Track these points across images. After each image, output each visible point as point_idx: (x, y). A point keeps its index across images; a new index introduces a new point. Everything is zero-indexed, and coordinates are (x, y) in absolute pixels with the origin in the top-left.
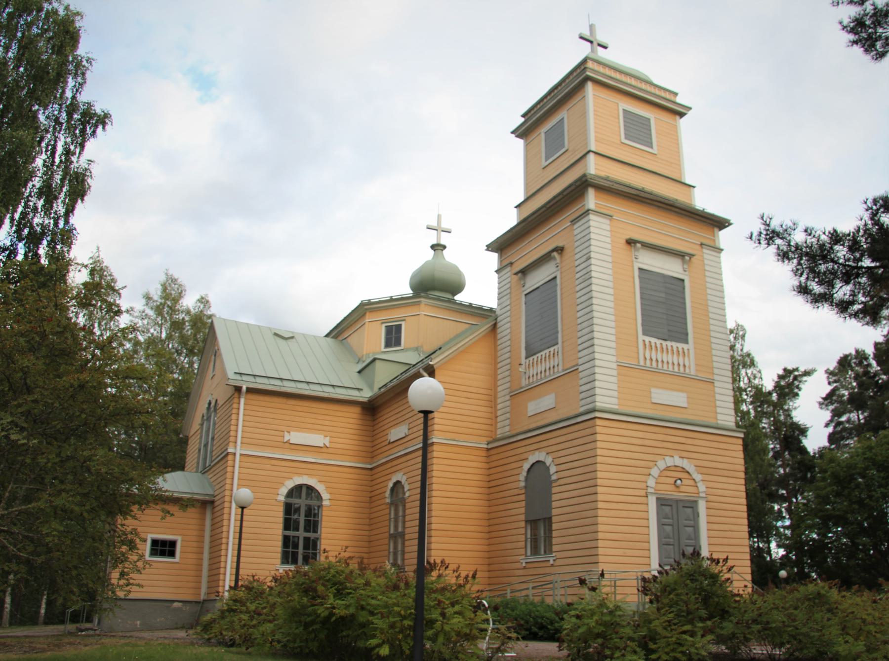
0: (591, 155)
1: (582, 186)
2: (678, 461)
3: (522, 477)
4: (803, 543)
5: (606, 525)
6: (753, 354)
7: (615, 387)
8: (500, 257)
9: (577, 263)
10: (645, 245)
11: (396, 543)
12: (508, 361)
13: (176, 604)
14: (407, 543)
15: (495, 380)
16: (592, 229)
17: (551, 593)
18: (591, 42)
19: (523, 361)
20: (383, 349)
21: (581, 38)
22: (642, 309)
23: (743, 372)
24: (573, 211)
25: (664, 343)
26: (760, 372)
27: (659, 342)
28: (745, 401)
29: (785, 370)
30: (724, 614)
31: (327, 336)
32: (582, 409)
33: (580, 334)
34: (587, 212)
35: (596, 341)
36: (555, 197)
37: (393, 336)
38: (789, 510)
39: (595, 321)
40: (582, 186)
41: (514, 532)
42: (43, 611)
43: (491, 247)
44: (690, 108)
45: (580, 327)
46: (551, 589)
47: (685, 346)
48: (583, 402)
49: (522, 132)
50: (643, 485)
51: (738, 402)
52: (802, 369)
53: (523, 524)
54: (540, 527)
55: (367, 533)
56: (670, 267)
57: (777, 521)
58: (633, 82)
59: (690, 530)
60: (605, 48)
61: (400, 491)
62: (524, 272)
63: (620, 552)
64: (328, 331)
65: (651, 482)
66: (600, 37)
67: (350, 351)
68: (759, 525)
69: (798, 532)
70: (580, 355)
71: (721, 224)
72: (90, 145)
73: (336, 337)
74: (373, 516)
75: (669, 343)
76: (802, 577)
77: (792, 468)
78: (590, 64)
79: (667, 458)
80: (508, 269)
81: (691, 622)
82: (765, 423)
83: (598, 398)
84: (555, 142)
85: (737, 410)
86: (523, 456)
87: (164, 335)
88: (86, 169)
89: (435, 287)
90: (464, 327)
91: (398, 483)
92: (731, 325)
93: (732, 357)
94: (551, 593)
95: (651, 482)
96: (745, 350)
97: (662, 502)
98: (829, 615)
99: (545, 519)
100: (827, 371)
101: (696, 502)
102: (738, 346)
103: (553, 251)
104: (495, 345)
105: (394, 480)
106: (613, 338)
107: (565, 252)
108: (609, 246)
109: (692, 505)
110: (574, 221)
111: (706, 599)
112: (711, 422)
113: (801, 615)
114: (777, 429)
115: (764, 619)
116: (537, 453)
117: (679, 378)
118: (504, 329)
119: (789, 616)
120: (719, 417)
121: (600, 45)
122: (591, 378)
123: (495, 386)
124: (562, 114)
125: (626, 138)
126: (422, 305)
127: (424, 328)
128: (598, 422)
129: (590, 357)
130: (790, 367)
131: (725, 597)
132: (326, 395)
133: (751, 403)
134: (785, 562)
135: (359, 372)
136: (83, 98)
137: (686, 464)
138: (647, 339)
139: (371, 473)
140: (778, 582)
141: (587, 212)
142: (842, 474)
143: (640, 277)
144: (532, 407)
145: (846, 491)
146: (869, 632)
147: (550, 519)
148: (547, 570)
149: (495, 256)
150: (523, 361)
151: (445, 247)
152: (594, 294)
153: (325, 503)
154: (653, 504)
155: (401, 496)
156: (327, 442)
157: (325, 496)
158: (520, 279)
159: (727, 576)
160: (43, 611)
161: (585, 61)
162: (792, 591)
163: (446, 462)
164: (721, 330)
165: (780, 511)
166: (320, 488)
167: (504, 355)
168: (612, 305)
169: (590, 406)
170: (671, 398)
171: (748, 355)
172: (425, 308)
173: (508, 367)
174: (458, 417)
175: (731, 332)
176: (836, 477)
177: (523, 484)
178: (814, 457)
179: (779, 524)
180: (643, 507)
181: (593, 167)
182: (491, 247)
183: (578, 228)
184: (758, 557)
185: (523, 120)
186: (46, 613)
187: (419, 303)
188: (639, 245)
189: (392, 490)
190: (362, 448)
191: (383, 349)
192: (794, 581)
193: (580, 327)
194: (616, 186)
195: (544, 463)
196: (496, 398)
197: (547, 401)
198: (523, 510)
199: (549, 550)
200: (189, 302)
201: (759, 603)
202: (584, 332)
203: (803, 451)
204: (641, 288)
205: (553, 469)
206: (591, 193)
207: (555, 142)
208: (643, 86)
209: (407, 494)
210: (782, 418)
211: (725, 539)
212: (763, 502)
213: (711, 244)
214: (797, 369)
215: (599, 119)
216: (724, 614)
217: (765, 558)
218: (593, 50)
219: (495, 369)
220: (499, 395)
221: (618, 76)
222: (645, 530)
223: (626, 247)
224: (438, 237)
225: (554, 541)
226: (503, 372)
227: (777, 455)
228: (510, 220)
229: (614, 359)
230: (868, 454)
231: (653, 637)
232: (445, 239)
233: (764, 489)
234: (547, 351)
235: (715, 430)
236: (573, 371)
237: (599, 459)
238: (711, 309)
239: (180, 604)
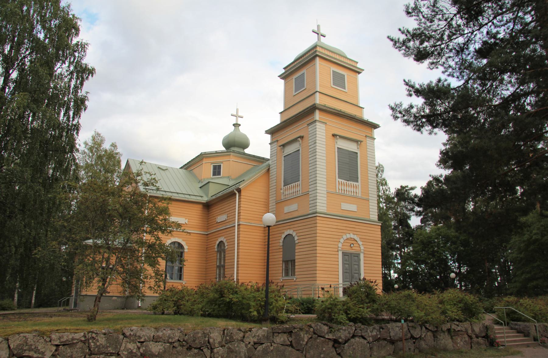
0: (318, 93)
1: (313, 109)
2: (352, 236)
3: (281, 241)
4: (406, 272)
5: (320, 264)
6: (386, 179)
7: (325, 202)
8: (272, 137)
9: (310, 144)
10: (341, 137)
11: (220, 270)
12: (275, 187)
13: (114, 298)
14: (226, 270)
15: (268, 196)
16: (317, 129)
17: (296, 293)
18: (318, 34)
19: (282, 187)
20: (212, 177)
21: (313, 32)
22: (338, 167)
23: (381, 188)
24: (308, 120)
25: (348, 182)
26: (389, 188)
27: (345, 182)
28: (381, 202)
29: (401, 187)
30: (374, 301)
31: (181, 168)
32: (310, 212)
33: (310, 177)
34: (315, 121)
35: (318, 181)
36: (300, 113)
37: (217, 170)
38: (400, 255)
39: (318, 172)
40: (313, 109)
41: (277, 266)
42: (33, 301)
43: (267, 132)
44: (363, 70)
45: (310, 174)
46: (296, 291)
47: (357, 184)
48: (311, 209)
49: (284, 77)
50: (336, 247)
51: (379, 202)
52: (410, 186)
53: (281, 262)
54: (290, 265)
55: (205, 265)
56: (351, 147)
57: (394, 260)
58: (337, 57)
59: (356, 266)
60: (324, 37)
61: (222, 245)
62: (284, 146)
63: (326, 276)
64: (182, 165)
65: (340, 245)
66: (322, 32)
67: (195, 176)
68: (387, 263)
69: (404, 267)
70: (310, 187)
71: (375, 126)
72: (86, 83)
73: (186, 169)
74: (207, 257)
75: (350, 182)
76: (405, 287)
77: (403, 235)
78: (318, 49)
79: (347, 235)
80: (276, 143)
81: (363, 304)
82: (390, 212)
83: (318, 207)
84: (300, 84)
85: (379, 207)
86: (282, 231)
87: (93, 163)
88: (85, 97)
89: (235, 144)
90: (251, 167)
91: (221, 242)
92: (377, 165)
93: (377, 181)
94: (296, 293)
95: (340, 245)
96: (383, 177)
97: (344, 254)
98: (412, 302)
99: (291, 261)
100: (421, 188)
101: (359, 254)
102: (379, 175)
103: (298, 138)
104: (269, 179)
105: (219, 240)
106: (325, 180)
107: (304, 139)
108: (325, 137)
109: (358, 256)
110: (309, 125)
111: (368, 295)
112: (367, 218)
113: (402, 302)
114: (397, 216)
115: (389, 303)
116: (289, 230)
117: (354, 198)
118: (273, 171)
119: (398, 302)
120: (371, 216)
121: (322, 35)
122: (315, 198)
123: (268, 198)
124: (304, 71)
125: (333, 85)
126: (231, 156)
127: (232, 167)
128: (318, 218)
129: (315, 188)
130: (404, 185)
131: (374, 295)
132: (187, 199)
133: (384, 203)
134: (397, 280)
135: (200, 188)
136: (84, 61)
137: (355, 237)
138: (340, 180)
139: (207, 237)
140: (394, 290)
141: (315, 121)
142: (425, 241)
143: (338, 152)
144: (287, 209)
145: (427, 249)
146: (427, 309)
147: (294, 260)
148: (293, 283)
149: (269, 136)
150: (282, 187)
151: (240, 125)
152: (317, 160)
153: (186, 250)
154: (343, 254)
155: (223, 248)
156: (187, 221)
157: (186, 247)
158: (282, 149)
159: (376, 287)
160: (33, 301)
161: (315, 47)
162: (399, 294)
163: (246, 233)
164: (373, 165)
165: (396, 255)
166: (183, 243)
167: (273, 183)
168: (325, 164)
169: (315, 211)
170: (350, 207)
171: (384, 180)
172: (233, 158)
173: (275, 189)
174: (253, 213)
175: (377, 168)
176: (422, 242)
177: (282, 244)
178: (413, 230)
179: (396, 261)
180: (336, 256)
181: (319, 100)
182: (267, 132)
183: (311, 128)
184: (385, 277)
185: (284, 71)
186: (35, 302)
187: (230, 155)
188: (338, 137)
189: (218, 245)
190: (200, 224)
191: (212, 177)
192: (400, 290)
193: (310, 174)
194: (329, 109)
195: (292, 235)
196: (268, 204)
197: (293, 207)
198: (281, 256)
199: (293, 274)
200: (106, 146)
201: (387, 298)
202: (312, 176)
203: (408, 226)
204: (338, 157)
205: (296, 238)
206: (317, 112)
207: (300, 84)
208: (342, 59)
209: (226, 247)
210: (399, 210)
211: (371, 270)
212: (388, 251)
213: (370, 136)
214: (407, 186)
215: (321, 74)
216: (374, 301)
217: (388, 278)
218: (319, 39)
219: (269, 190)
220: (270, 202)
221: (331, 54)
222: (337, 266)
223: (332, 137)
224: (237, 120)
225: (296, 270)
226: (272, 192)
227: (396, 228)
228: (276, 121)
229: (325, 189)
230: (438, 232)
231: (349, 309)
232: (240, 121)
233: (389, 245)
234: (294, 184)
235: (367, 222)
236: (307, 194)
237: (318, 235)
238: (369, 167)
239: (116, 298)
